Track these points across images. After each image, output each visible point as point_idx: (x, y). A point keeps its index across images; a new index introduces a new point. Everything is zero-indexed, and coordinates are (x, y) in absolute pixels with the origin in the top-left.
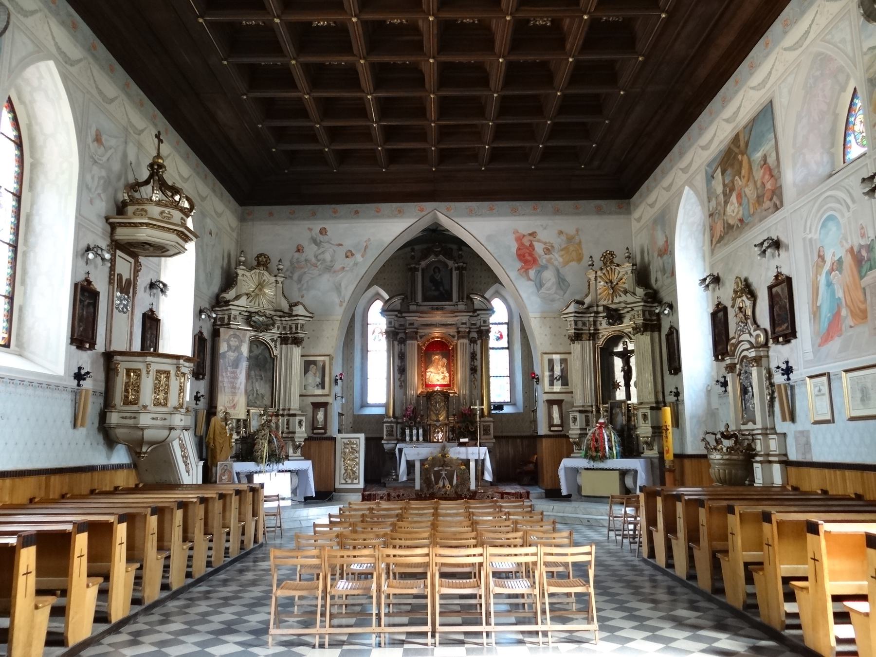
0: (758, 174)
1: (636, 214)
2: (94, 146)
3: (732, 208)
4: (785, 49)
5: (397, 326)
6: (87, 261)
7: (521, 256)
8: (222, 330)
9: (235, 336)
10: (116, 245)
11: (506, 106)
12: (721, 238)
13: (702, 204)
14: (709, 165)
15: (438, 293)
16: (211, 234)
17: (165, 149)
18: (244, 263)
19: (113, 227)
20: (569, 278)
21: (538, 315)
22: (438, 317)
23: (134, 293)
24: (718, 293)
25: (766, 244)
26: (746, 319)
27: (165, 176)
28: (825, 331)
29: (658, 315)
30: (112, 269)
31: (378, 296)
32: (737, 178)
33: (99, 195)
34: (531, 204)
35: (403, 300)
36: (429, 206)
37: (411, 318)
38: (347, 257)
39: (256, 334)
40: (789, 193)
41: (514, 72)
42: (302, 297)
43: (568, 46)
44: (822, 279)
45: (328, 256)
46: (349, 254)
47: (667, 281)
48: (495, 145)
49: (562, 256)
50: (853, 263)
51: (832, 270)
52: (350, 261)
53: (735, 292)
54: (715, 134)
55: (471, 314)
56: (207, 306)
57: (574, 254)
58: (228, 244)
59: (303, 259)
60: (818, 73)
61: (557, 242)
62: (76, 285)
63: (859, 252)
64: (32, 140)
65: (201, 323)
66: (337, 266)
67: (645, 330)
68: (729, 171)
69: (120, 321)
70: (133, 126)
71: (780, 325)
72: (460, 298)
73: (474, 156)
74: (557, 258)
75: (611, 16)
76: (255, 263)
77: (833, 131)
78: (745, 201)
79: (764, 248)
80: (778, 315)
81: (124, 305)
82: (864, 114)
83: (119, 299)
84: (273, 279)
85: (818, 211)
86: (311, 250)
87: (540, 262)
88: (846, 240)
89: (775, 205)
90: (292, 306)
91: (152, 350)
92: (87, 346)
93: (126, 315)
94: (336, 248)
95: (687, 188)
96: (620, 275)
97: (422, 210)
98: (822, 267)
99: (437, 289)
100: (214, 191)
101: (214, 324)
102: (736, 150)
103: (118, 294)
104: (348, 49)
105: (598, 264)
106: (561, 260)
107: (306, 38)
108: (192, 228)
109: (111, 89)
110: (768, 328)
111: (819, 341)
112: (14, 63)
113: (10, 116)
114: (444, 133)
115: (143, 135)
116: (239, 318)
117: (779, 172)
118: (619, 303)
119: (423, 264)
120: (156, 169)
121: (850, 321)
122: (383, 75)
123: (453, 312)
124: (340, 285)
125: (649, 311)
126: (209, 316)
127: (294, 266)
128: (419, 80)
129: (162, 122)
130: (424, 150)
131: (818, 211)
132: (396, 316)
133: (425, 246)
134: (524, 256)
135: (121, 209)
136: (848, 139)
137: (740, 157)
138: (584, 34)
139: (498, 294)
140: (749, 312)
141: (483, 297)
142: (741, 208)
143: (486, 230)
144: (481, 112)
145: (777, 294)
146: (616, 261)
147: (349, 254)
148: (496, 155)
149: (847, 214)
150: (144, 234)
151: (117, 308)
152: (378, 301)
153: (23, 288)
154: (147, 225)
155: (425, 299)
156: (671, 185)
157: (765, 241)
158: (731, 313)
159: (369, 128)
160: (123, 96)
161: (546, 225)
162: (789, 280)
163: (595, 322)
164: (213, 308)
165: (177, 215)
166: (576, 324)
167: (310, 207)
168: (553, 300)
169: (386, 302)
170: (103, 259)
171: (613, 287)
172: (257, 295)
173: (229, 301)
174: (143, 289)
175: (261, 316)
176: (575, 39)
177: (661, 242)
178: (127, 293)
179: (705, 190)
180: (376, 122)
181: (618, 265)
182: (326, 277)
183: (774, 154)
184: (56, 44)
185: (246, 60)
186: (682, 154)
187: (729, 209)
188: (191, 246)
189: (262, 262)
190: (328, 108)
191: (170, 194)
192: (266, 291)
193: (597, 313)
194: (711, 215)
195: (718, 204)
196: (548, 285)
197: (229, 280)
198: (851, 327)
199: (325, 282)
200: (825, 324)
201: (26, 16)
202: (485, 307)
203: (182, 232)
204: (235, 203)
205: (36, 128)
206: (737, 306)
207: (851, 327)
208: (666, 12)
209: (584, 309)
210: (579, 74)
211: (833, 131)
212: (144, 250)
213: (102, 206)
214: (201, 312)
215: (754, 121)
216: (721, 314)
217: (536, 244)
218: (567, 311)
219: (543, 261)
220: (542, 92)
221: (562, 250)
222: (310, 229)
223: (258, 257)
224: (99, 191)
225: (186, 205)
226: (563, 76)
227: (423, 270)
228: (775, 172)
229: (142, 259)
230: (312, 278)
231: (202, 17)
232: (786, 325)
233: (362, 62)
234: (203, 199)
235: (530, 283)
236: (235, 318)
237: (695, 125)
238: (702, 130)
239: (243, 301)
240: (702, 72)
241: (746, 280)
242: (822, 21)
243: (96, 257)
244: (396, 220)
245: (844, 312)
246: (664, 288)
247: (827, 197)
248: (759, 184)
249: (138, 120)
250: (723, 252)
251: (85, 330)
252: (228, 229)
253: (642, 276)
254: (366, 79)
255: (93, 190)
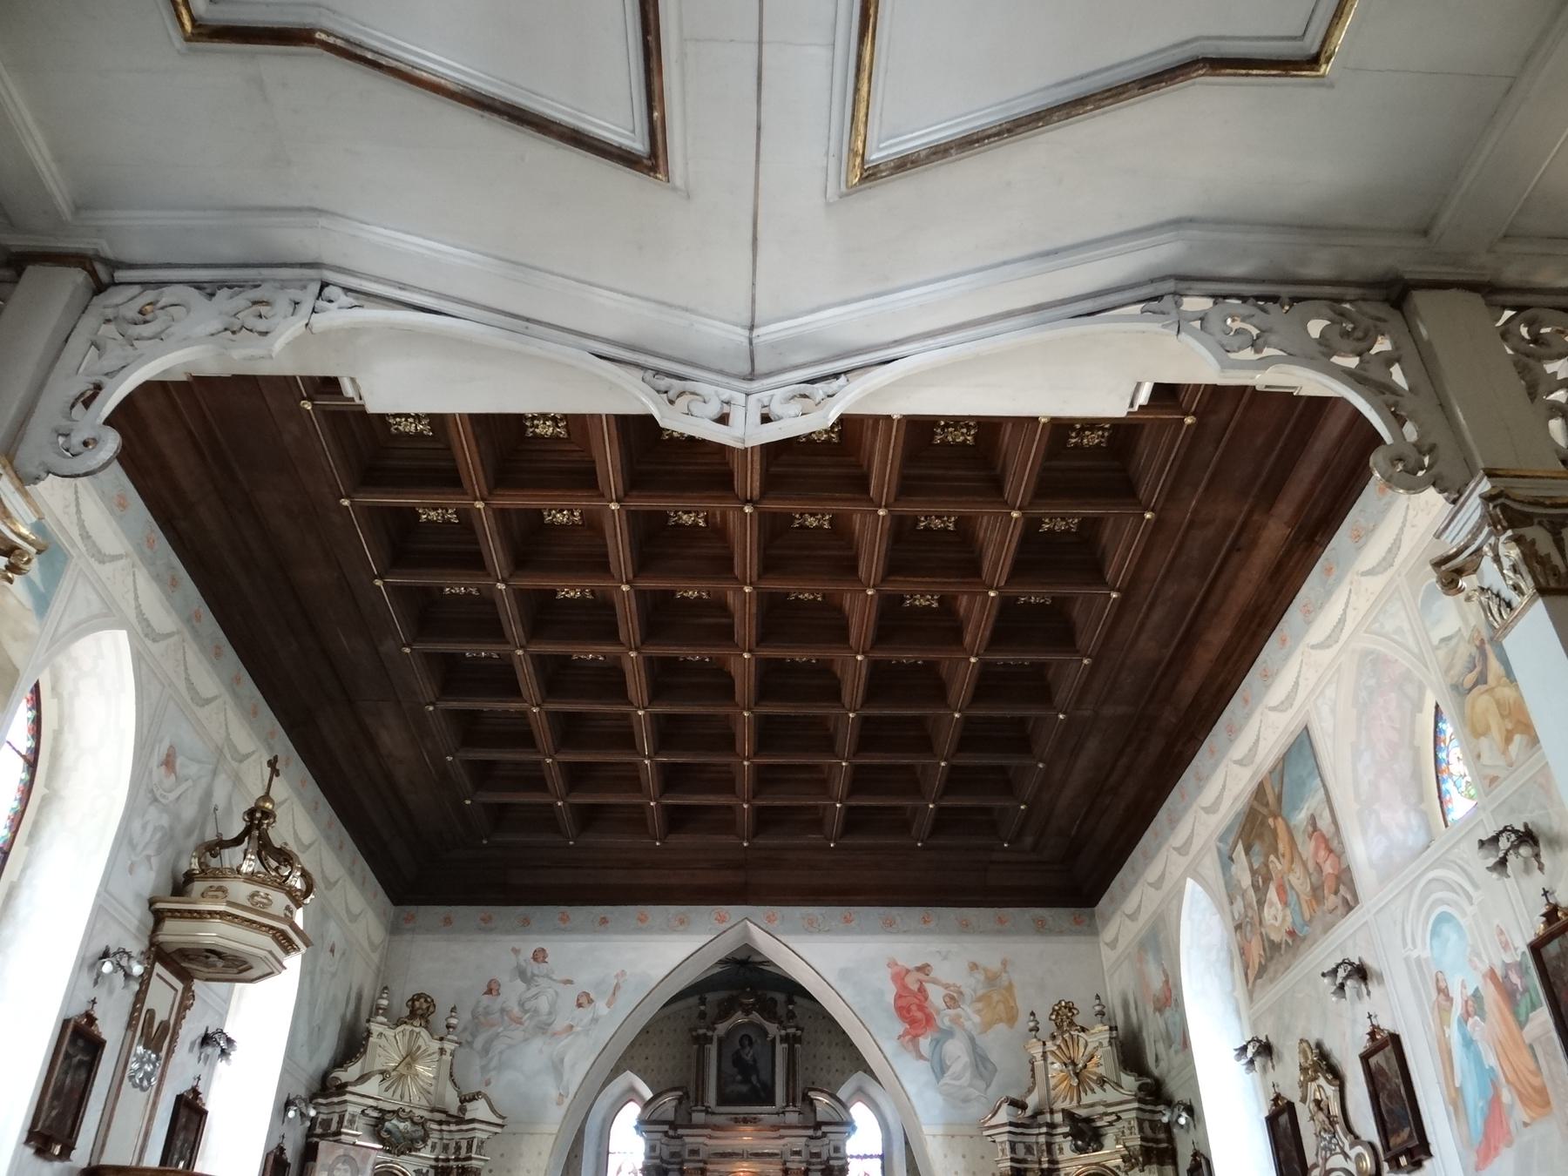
0: (1307, 848)
1: (1108, 934)
2: (159, 773)
3: (1273, 911)
4: (1313, 647)
5: (666, 1155)
6: (98, 979)
7: (903, 1011)
8: (323, 1145)
9: (347, 1159)
10: (158, 953)
11: (871, 735)
12: (1262, 970)
13: (1220, 909)
14: (1222, 839)
15: (747, 1088)
16: (332, 951)
17: (280, 789)
18: (386, 1011)
19: (159, 917)
20: (994, 1057)
21: (939, 1130)
22: (746, 1138)
23: (170, 1051)
24: (1272, 1076)
25: (1341, 973)
26: (1332, 1123)
27: (271, 833)
28: (1480, 1137)
29: (1168, 1128)
30: (140, 997)
31: (631, 1094)
32: (1272, 857)
33: (148, 858)
34: (918, 912)
35: (680, 1100)
36: (735, 912)
37: (693, 1139)
38: (580, 1005)
39: (388, 1158)
40: (1364, 878)
41: (882, 681)
42: (488, 1083)
43: (968, 639)
44: (1454, 1034)
45: (543, 1004)
46: (584, 1000)
47: (1177, 1060)
48: (853, 803)
49: (978, 1012)
50: (1498, 997)
51: (1467, 1015)
52: (586, 1014)
53: (1304, 1070)
54: (1224, 787)
55: (810, 1132)
56: (303, 1093)
57: (1001, 1007)
58: (362, 976)
59: (496, 1006)
60: (1372, 682)
61: (970, 984)
62: (66, 1023)
63: (1506, 976)
64: (55, 756)
65: (284, 1129)
66: (560, 1024)
67: (1147, 1162)
68: (1257, 848)
69: (133, 1101)
70: (233, 748)
71: (1396, 1132)
72: (790, 1099)
73: (815, 821)
74: (971, 1016)
75: (1034, 595)
76: (406, 1012)
77: (1417, 775)
78: (1292, 898)
79: (1339, 980)
80: (1390, 1112)
81: (146, 1073)
82: (1461, 745)
83: (140, 1059)
84: (436, 1045)
85: (1420, 907)
86: (513, 991)
87: (939, 1022)
88: (1479, 955)
89: (1346, 901)
90: (465, 1100)
91: (181, 1164)
92: (57, 1150)
93: (144, 1095)
94: (560, 988)
95: (1190, 882)
96: (1089, 1049)
97: (722, 920)
98: (1449, 1011)
99: (746, 1081)
100: (352, 873)
101: (310, 1132)
102: (1264, 811)
103: (140, 1049)
104: (610, 633)
105: (1047, 1027)
106: (977, 1019)
107: (544, 614)
108: (301, 926)
109: (208, 683)
110: (1375, 1139)
111: (1473, 1158)
112: (62, 629)
113: (31, 714)
114: (765, 778)
115: (247, 758)
116: (361, 1122)
117: (1341, 842)
118: (1092, 1105)
119: (722, 1028)
120: (258, 818)
121: (1520, 1114)
122: (664, 678)
123: (776, 1128)
124: (562, 1061)
125: (1151, 1122)
126: (302, 1114)
127: (479, 1021)
128: (724, 687)
129: (284, 745)
130: (729, 808)
131: (1420, 907)
132: (666, 1133)
133: (723, 994)
134: (909, 1011)
135: (181, 885)
136: (1444, 787)
137: (1271, 821)
138: (991, 620)
139: (861, 1094)
140: (1335, 1109)
141: (833, 1096)
142: (1288, 912)
143: (839, 959)
144: (827, 744)
145: (1380, 1069)
146: (1078, 1020)
147: (584, 1000)
148: (855, 821)
149: (1470, 910)
150: (213, 934)
151: (131, 1078)
152: (631, 1104)
153: (27, 849)
154: (222, 915)
155: (723, 1100)
156: (1162, 877)
157: (1338, 966)
158: (1303, 1113)
159: (635, 767)
160: (227, 697)
161: (947, 952)
162: (1395, 1040)
163: (1049, 1145)
164: (311, 1099)
165: (280, 900)
166: (1013, 1150)
167: (522, 909)
168: (966, 1100)
169: (646, 1105)
170: (128, 976)
171: (1078, 1072)
172: (402, 1076)
173: (346, 1085)
174: (187, 1045)
175: (404, 1120)
176: (978, 629)
177: (1157, 983)
178: (157, 1050)
179: (1221, 882)
180: (649, 757)
181: (1083, 1030)
182: (537, 1043)
183: (1327, 813)
184: (138, 607)
185: (442, 647)
186: (1173, 823)
187: (1268, 913)
188: (294, 962)
189: (420, 1010)
190: (570, 730)
191: (274, 864)
192: (420, 1068)
193: (1052, 1126)
194: (1238, 927)
195: (1247, 906)
196: (956, 1068)
197: (352, 1045)
198: (1526, 1125)
199: (534, 1054)
200: (1477, 1122)
201: (102, 562)
202: (837, 1119)
203: (283, 933)
204: (386, 899)
205: (68, 737)
206: (1310, 1097)
207: (1526, 1125)
208: (1118, 590)
209: (1026, 1119)
210: (989, 684)
211: (1417, 775)
212: (207, 965)
213: (148, 879)
214: (288, 1104)
215: (1285, 760)
216: (1284, 1119)
217: (929, 987)
218: (994, 1122)
219: (944, 1020)
220: (928, 712)
221: (979, 1000)
222: (516, 951)
223: (413, 1000)
224: (150, 851)
225: (298, 884)
226: (961, 686)
227: (720, 1040)
228: (1334, 844)
229: (197, 985)
230: (510, 1047)
231: (381, 578)
232: (1407, 1130)
233: (633, 654)
234: (330, 885)
235: (921, 1062)
236: (352, 1122)
237: (1189, 774)
238: (1202, 781)
239: (372, 1087)
240: (1189, 686)
241: (1319, 1045)
242: (1361, 604)
243: (115, 971)
244: (675, 937)
245: (1506, 1096)
246: (1173, 1073)
247: (1430, 881)
248: (1311, 866)
249: (243, 739)
250: (1270, 994)
251: (61, 1116)
252: (366, 944)
253: (1130, 1053)
254: (637, 685)
255: (140, 848)
